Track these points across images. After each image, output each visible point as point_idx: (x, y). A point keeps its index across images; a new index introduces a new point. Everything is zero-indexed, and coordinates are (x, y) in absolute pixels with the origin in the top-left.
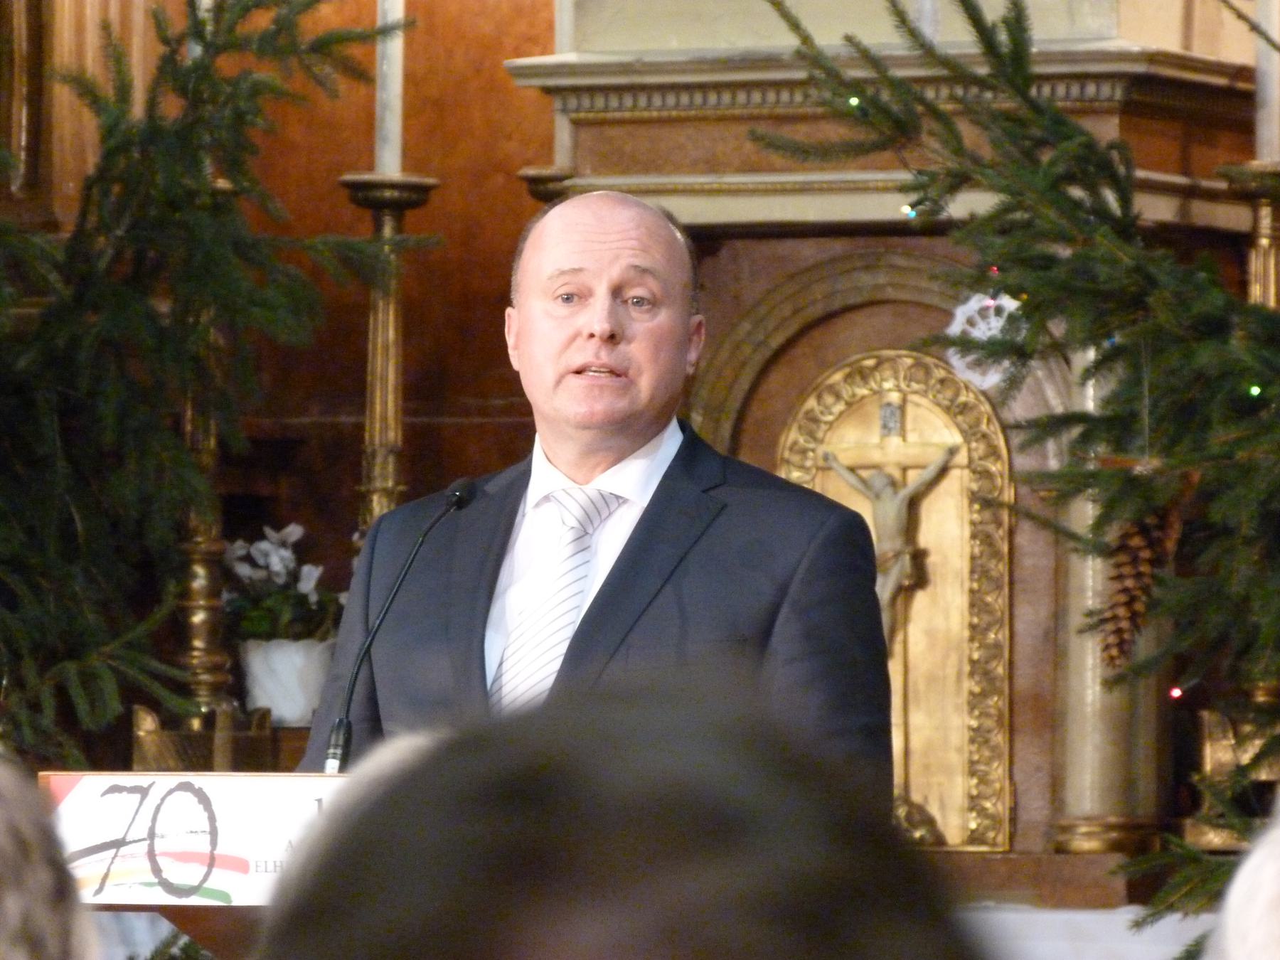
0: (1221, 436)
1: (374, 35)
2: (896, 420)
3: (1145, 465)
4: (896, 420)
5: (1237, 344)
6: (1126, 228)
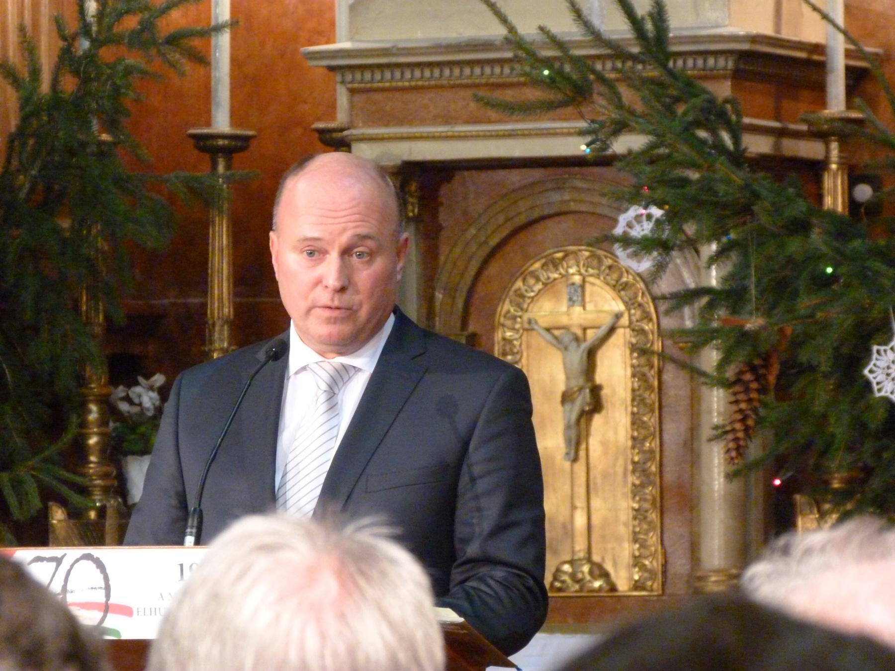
0: (805, 303)
1: (209, 31)
2: (578, 295)
3: (753, 323)
4: (578, 295)
5: (816, 237)
6: (738, 158)
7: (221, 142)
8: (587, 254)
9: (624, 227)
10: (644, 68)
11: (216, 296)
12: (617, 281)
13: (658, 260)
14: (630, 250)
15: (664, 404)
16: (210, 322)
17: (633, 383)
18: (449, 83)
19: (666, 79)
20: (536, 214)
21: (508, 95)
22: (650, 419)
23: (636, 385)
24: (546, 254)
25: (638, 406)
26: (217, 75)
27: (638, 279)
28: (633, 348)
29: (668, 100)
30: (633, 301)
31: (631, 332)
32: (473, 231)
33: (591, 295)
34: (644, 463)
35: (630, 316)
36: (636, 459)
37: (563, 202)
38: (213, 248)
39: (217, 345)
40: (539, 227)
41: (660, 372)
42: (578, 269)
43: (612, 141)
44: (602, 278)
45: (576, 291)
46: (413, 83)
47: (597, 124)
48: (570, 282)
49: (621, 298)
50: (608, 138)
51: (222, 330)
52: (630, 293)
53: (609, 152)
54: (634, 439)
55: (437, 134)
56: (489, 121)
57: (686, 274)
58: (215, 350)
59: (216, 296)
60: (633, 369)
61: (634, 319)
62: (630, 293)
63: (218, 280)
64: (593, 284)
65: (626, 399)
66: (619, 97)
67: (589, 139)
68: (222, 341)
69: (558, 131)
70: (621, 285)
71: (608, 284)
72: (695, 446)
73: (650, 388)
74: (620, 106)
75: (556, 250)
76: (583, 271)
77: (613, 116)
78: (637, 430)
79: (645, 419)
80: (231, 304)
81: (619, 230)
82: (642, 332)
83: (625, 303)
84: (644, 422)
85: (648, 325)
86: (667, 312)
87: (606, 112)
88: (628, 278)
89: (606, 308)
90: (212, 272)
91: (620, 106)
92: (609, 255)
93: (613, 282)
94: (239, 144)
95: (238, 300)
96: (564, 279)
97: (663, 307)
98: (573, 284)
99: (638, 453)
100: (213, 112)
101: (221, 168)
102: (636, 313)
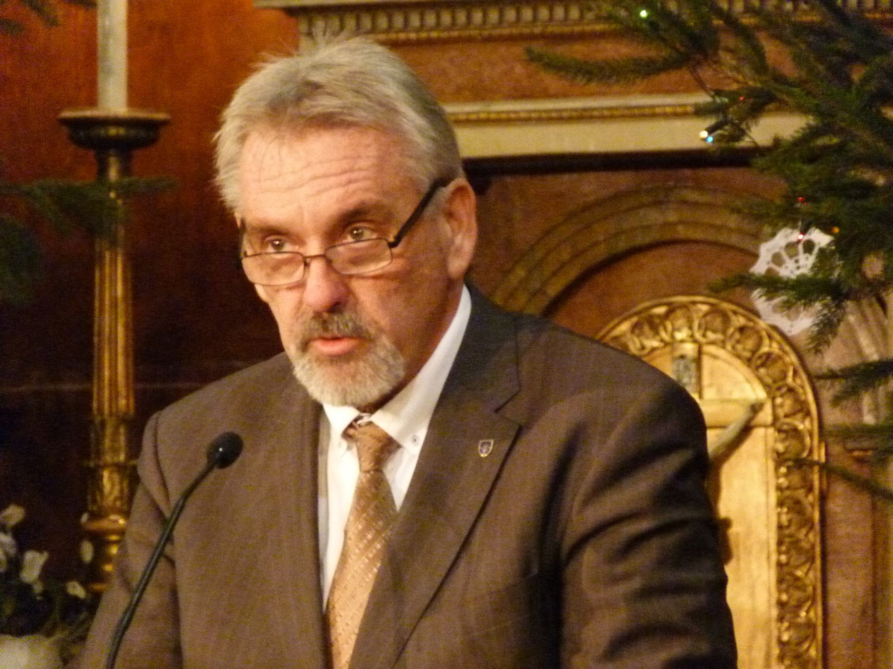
7: (113, 131)
8: (705, 308)
9: (768, 263)
10: (796, 8)
11: (106, 381)
12: (754, 352)
13: (825, 315)
14: (777, 300)
15: (829, 549)
16: (98, 420)
17: (779, 515)
18: (480, 35)
19: (831, 23)
20: (622, 245)
21: (578, 51)
22: (807, 574)
23: (784, 519)
24: (640, 307)
25: (787, 552)
26: (107, 23)
27: (787, 348)
28: (780, 459)
29: (835, 59)
31: (776, 434)
32: (521, 272)
33: (712, 374)
34: (799, 644)
35: (774, 407)
36: (785, 637)
37: (667, 224)
38: (102, 300)
39: (108, 458)
40: (627, 268)
41: (823, 498)
42: (690, 333)
43: (750, 124)
44: (729, 347)
45: (687, 368)
46: (424, 35)
47: (726, 96)
48: (678, 353)
49: (761, 380)
50: (742, 119)
51: (116, 433)
52: (775, 370)
53: (745, 143)
54: (781, 604)
55: (462, 117)
56: (547, 95)
57: (864, 340)
58: (105, 466)
59: (106, 381)
60: (779, 493)
61: (781, 412)
62: (775, 370)
63: (110, 353)
64: (715, 357)
65: (768, 543)
66: (759, 52)
67: (711, 121)
68: (115, 451)
69: (658, 110)
70: (760, 357)
71: (739, 357)
72: (879, 614)
73: (807, 523)
74: (760, 65)
75: (656, 302)
76: (698, 335)
77: (751, 83)
78: (787, 591)
79: (799, 573)
80: (131, 393)
81: (760, 268)
82: (794, 433)
83: (766, 386)
84: (797, 579)
85: (803, 422)
86: (837, 401)
87: (740, 78)
88: (770, 346)
89: (736, 395)
90: (100, 341)
91: (760, 65)
92: (741, 310)
93: (747, 354)
94: (142, 133)
95: (140, 386)
96: (668, 349)
97: (827, 395)
98: (682, 357)
99: (788, 629)
100: (100, 85)
101: (113, 174)
102: (786, 404)
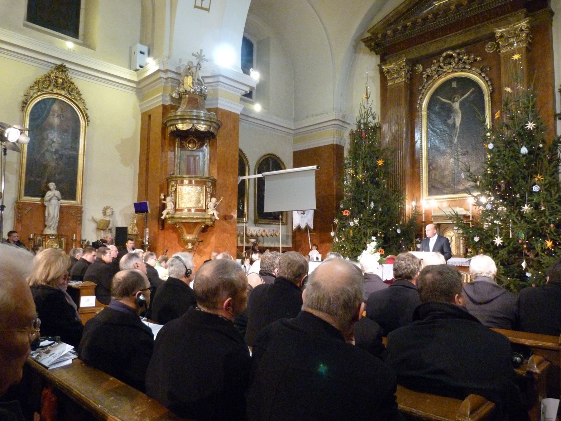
0: (469, 234)
4: (451, 233)
6: (464, 223)
19: (352, 300)
30: (372, 154)
